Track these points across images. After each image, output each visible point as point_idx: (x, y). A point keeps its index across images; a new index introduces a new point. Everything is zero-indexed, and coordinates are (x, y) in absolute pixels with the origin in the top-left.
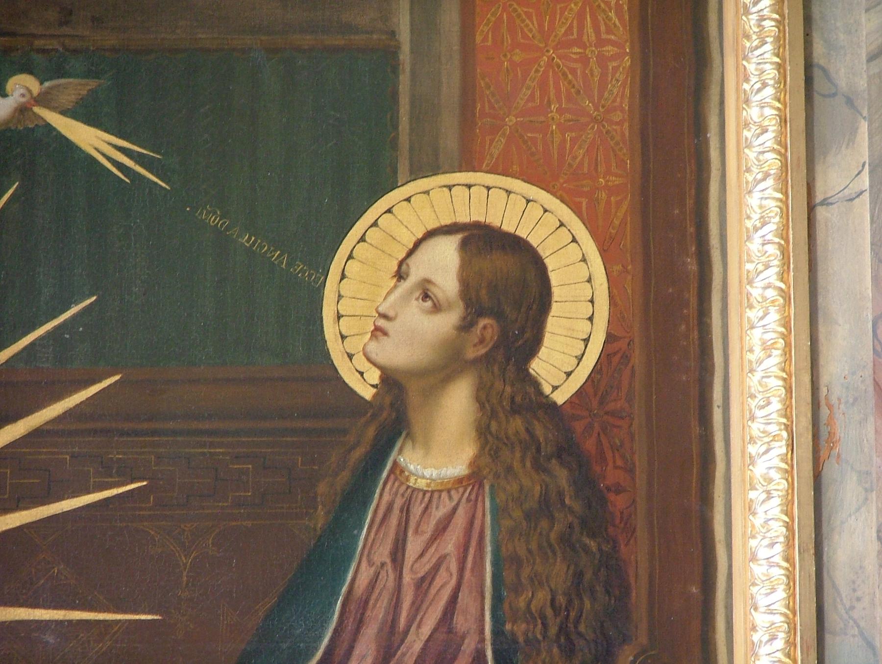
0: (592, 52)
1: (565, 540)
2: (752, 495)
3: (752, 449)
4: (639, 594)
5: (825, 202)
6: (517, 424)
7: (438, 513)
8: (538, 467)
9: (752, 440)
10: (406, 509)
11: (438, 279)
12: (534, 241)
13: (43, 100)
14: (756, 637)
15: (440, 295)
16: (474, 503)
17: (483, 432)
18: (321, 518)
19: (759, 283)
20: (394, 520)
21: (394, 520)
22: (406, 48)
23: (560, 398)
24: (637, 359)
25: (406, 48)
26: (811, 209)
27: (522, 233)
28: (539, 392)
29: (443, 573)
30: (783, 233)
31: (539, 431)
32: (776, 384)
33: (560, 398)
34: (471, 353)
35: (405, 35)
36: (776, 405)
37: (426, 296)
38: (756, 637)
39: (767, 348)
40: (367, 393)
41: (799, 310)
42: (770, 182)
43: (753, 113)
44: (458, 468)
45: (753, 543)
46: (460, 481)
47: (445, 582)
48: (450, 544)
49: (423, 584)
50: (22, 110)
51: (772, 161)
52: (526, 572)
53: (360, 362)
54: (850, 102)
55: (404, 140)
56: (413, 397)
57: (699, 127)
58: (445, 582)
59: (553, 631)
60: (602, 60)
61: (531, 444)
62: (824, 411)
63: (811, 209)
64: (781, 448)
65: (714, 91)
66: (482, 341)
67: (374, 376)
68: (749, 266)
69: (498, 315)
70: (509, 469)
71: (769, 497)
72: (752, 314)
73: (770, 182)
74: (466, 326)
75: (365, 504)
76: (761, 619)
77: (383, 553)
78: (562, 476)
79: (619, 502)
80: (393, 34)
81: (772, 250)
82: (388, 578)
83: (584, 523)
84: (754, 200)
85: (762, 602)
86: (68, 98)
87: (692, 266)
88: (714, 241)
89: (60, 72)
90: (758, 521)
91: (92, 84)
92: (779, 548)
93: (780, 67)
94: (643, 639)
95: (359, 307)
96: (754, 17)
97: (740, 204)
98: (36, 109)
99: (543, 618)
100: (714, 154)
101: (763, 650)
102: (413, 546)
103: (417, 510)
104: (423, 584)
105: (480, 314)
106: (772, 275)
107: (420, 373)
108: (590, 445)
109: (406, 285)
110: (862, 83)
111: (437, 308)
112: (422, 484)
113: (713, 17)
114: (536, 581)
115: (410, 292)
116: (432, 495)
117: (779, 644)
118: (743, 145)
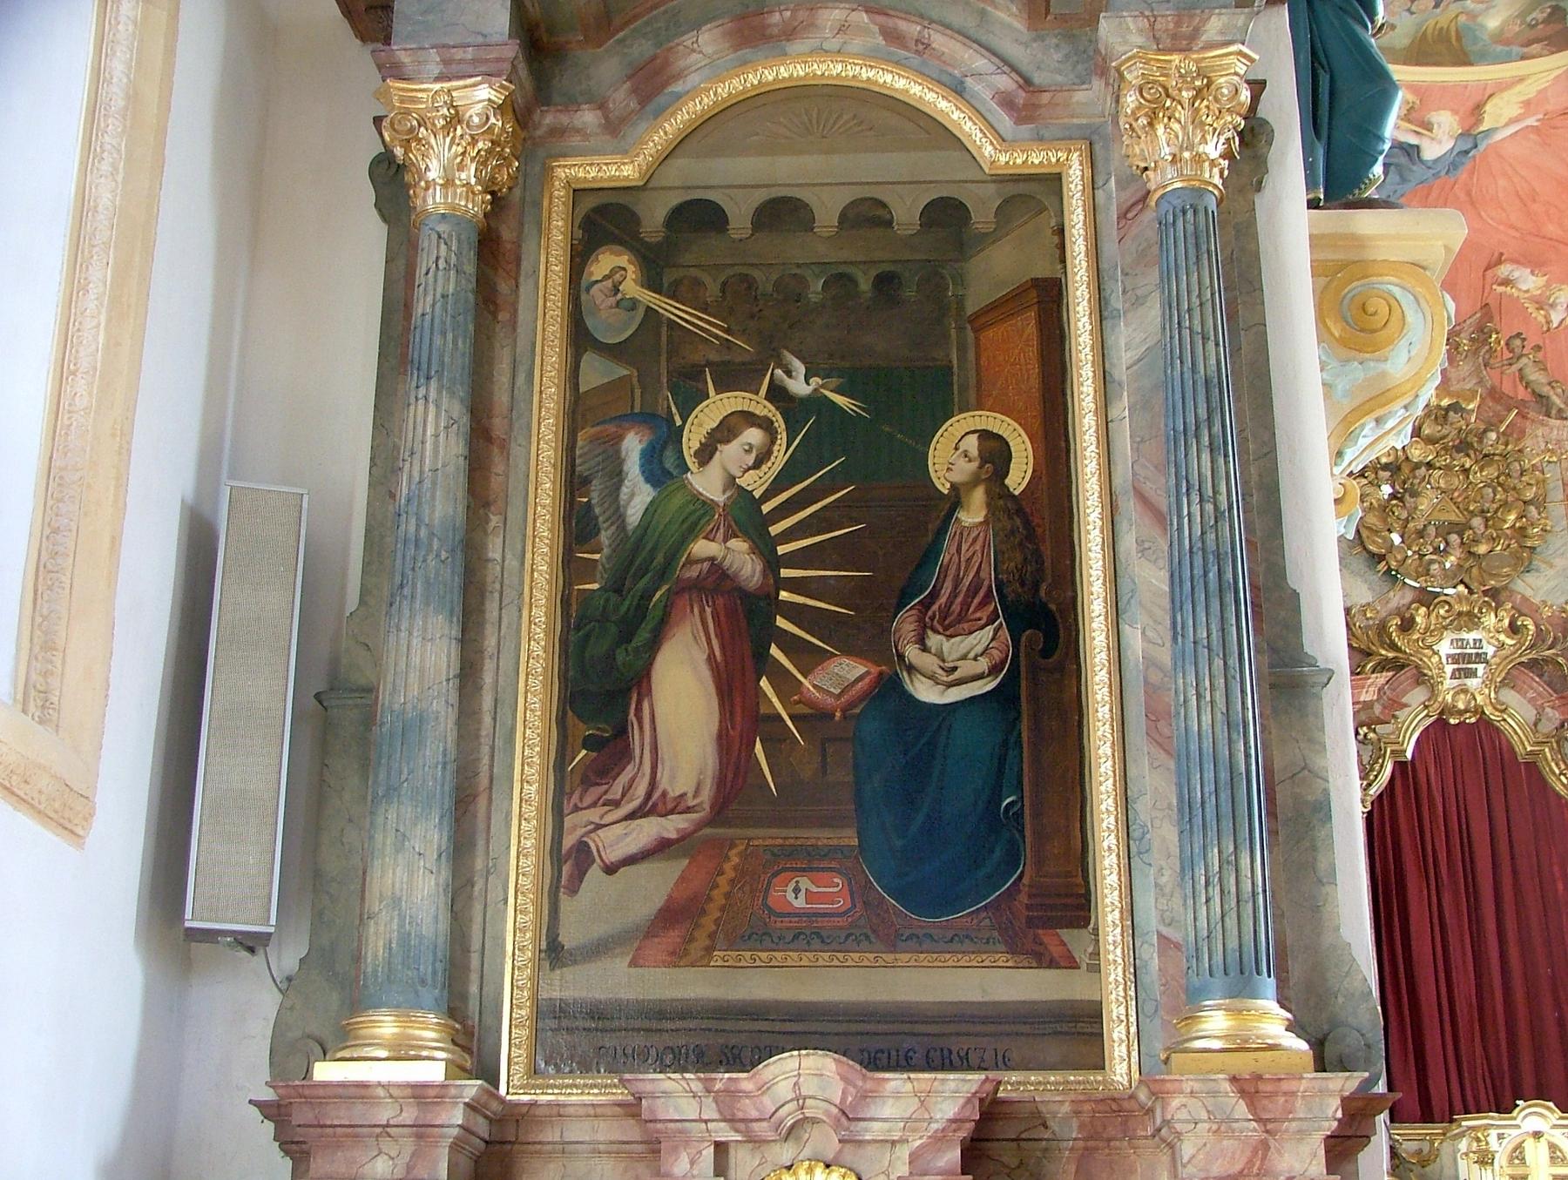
0: (1024, 368)
1: (1020, 544)
2: (1088, 527)
3: (1088, 511)
4: (1048, 564)
5: (1112, 421)
6: (1001, 502)
7: (973, 535)
8: (1010, 518)
9: (1088, 508)
10: (961, 534)
11: (970, 450)
12: (1005, 436)
13: (822, 386)
14: (1091, 579)
15: (971, 455)
16: (986, 531)
17: (988, 505)
18: (930, 538)
19: (1089, 450)
20: (957, 537)
21: (957, 537)
22: (955, 366)
23: (1017, 493)
24: (1044, 479)
25: (955, 366)
26: (1107, 423)
27: (1000, 433)
28: (1009, 490)
29: (975, 557)
30: (1097, 431)
31: (1009, 505)
32: (1097, 488)
33: (1017, 493)
34: (983, 477)
35: (955, 362)
36: (1096, 495)
37: (966, 456)
38: (1091, 579)
39: (1093, 474)
40: (946, 492)
41: (1104, 460)
42: (1092, 414)
43: (1084, 389)
44: (980, 519)
45: (1089, 545)
46: (981, 523)
47: (977, 560)
48: (978, 547)
49: (969, 560)
50: (815, 390)
51: (1092, 406)
52: (1006, 556)
53: (943, 480)
54: (1120, 385)
55: (956, 400)
56: (962, 494)
57: (1064, 394)
58: (977, 560)
59: (1016, 578)
60: (1027, 370)
61: (1007, 511)
62: (1114, 498)
63: (1107, 423)
64: (1099, 510)
65: (1069, 381)
66: (987, 472)
67: (948, 485)
68: (1084, 444)
69: (993, 463)
70: (999, 519)
71: (1111, 873)
72: (1086, 462)
73: (1092, 414)
74: (981, 467)
75: (947, 532)
76: (1093, 572)
77: (953, 550)
78: (1018, 521)
79: (1039, 530)
80: (950, 362)
81: (1093, 439)
82: (956, 558)
83: (1026, 538)
84: (1086, 421)
85: (1094, 566)
86: (832, 386)
87: (1063, 444)
88: (1084, 704)
89: (828, 377)
90: (1091, 537)
91: (841, 380)
92: (1099, 547)
93: (1094, 372)
94: (1050, 581)
95: (941, 460)
96: (1083, 354)
97: (1081, 422)
98: (822, 390)
99: (1013, 572)
100: (1075, 510)
101: (1095, 584)
102: (964, 548)
103: (965, 534)
104: (969, 560)
105: (986, 462)
106: (1093, 447)
107: (964, 484)
108: (1028, 510)
109: (958, 452)
110: (1125, 378)
111: (970, 461)
112: (967, 525)
113: (1078, 574)
114: (1010, 559)
115: (959, 456)
116: (970, 529)
117: (1101, 581)
118: (1111, 1031)
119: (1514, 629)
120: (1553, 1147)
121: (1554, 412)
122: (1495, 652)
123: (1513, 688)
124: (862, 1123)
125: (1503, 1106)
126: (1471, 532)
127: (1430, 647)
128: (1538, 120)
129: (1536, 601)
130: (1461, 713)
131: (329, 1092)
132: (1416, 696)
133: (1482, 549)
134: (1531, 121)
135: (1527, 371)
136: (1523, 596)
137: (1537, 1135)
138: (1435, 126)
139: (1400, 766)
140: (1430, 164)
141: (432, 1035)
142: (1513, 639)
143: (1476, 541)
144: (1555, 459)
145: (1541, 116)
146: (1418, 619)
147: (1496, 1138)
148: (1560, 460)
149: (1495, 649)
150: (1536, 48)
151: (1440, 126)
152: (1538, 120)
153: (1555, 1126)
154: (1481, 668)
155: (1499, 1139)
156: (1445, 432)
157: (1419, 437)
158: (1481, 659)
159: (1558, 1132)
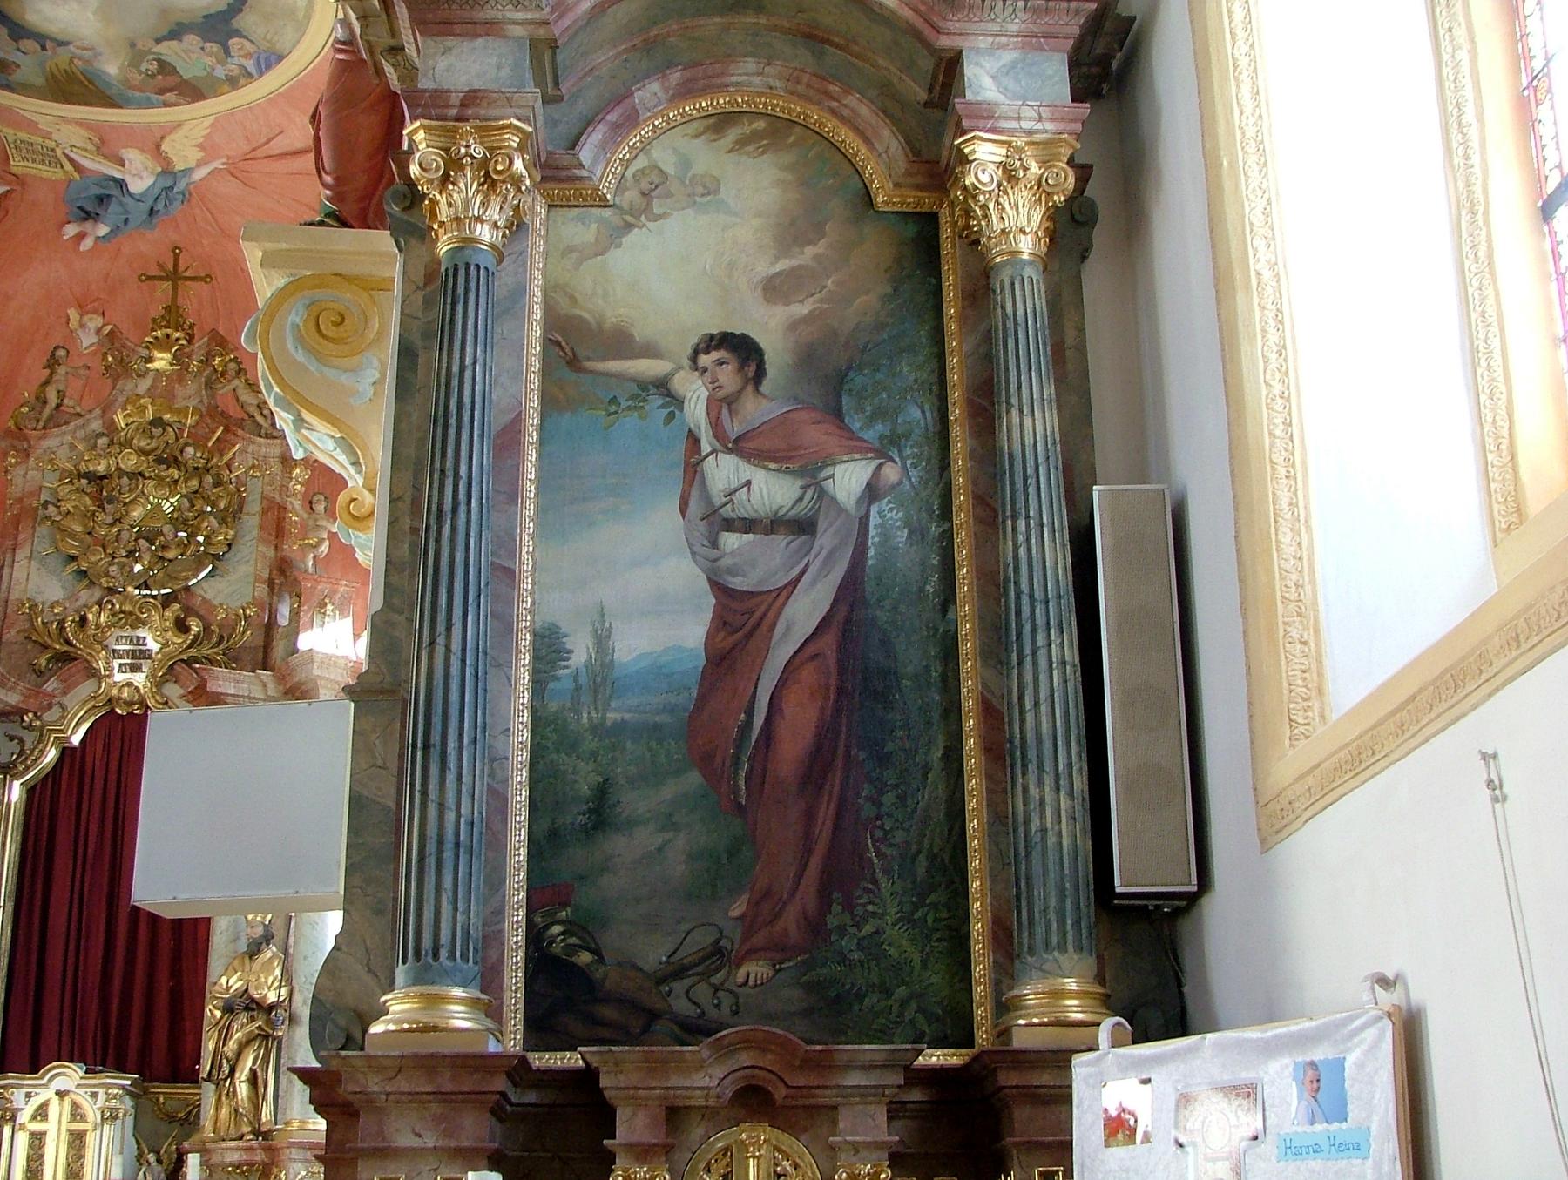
119: (181, 626)
120: (75, 1106)
121: (263, 431)
122: (161, 649)
123: (175, 682)
124: (430, 1090)
125: (34, 1067)
126: (162, 538)
127: (99, 643)
128: (224, 164)
129: (216, 603)
130: (130, 703)
131: (1032, 1057)
132: (86, 688)
133: (170, 554)
134: (217, 164)
135: (240, 392)
136: (204, 598)
137: (61, 1094)
138: (127, 162)
139: (66, 752)
140: (138, 197)
141: (462, 1008)
142: (179, 637)
143: (164, 547)
144: (258, 474)
145: (224, 160)
146: (90, 616)
147: (24, 1096)
148: (263, 475)
149: (159, 646)
150: (170, 97)
151: (131, 163)
152: (224, 164)
153: (79, 1086)
154: (146, 666)
155: (26, 1096)
156: (154, 445)
157: (132, 448)
158: (146, 654)
159: (81, 1091)
